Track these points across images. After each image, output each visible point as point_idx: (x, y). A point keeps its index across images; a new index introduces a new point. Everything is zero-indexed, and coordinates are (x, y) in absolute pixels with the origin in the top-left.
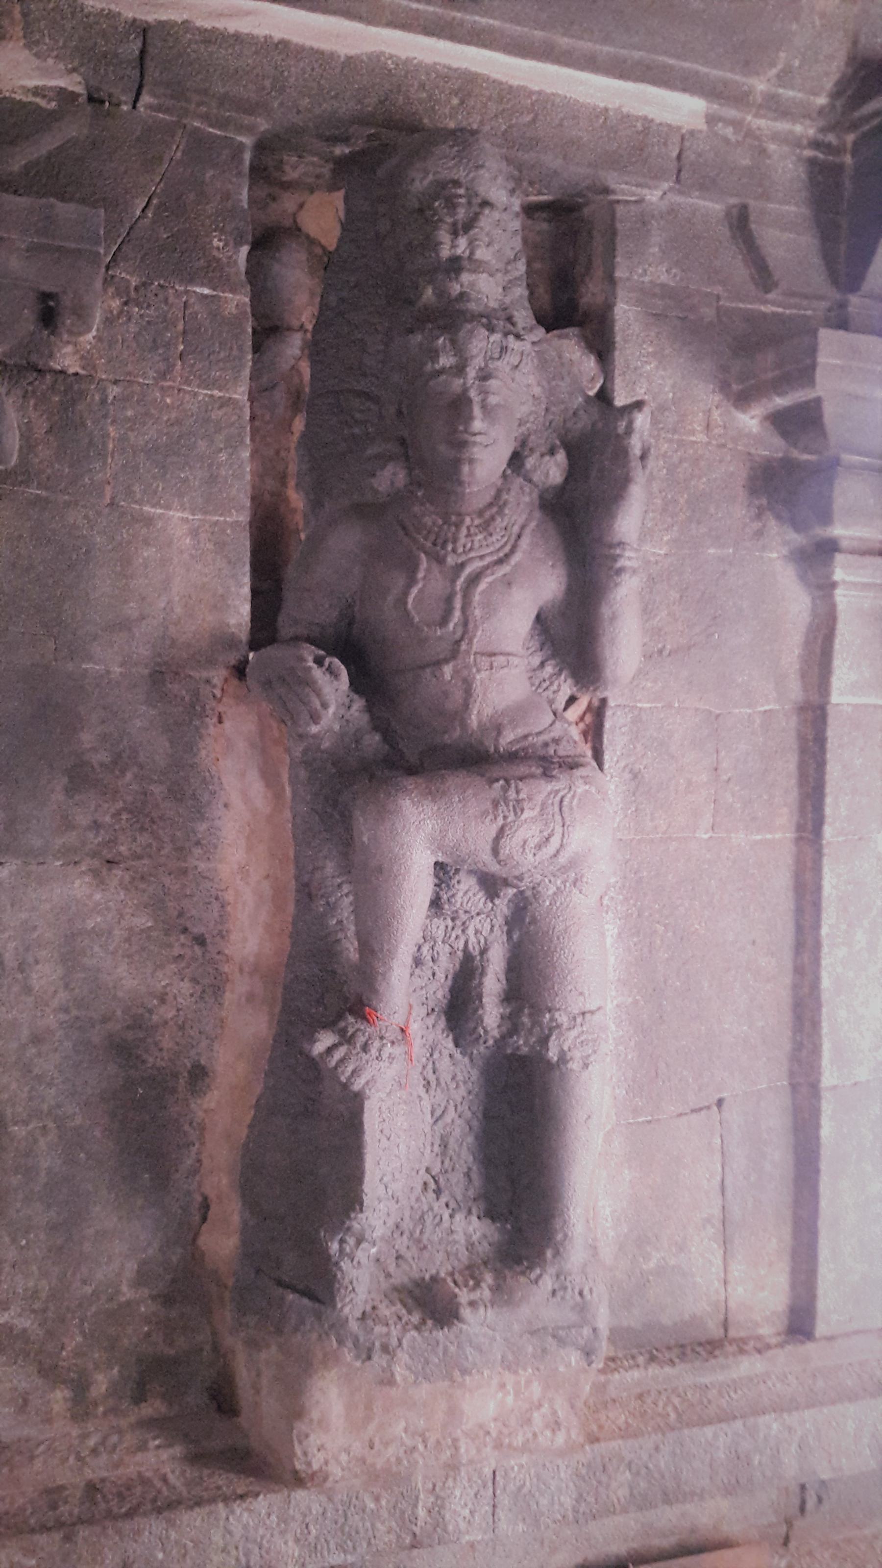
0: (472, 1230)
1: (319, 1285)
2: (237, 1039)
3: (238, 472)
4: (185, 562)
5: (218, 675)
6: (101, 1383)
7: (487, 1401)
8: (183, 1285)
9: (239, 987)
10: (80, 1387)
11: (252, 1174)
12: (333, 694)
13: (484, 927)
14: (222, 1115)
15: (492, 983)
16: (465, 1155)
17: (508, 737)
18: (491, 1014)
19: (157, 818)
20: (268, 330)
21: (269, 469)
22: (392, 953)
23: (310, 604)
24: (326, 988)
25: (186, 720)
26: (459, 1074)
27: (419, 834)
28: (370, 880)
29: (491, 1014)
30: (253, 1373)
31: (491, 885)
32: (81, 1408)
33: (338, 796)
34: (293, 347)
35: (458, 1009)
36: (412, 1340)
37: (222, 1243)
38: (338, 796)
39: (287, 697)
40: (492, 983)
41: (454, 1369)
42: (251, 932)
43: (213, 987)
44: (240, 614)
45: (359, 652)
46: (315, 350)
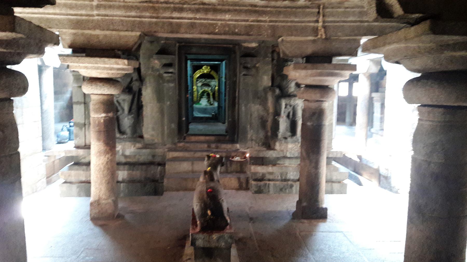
0: (289, 134)
1: (277, 136)
2: (270, 120)
3: (270, 73)
4: (266, 81)
5: (268, 89)
6: (260, 144)
7: (290, 146)
8: (266, 137)
9: (270, 114)
10: (259, 144)
11: (271, 129)
12: (277, 91)
13: (290, 109)
14: (269, 124)
15: (291, 114)
16: (289, 128)
17: (292, 94)
18: (291, 116)
19: (264, 102)
20: (273, 60)
21: (273, 71)
22: (233, 40)
23: (276, 83)
24: (277, 113)
25: (266, 93)
26: (289, 122)
27: (283, 103)
28: (280, 105)
29: (291, 116)
30: (272, 143)
31: (291, 106)
32: (259, 146)
33: (277, 99)
34: (275, 61)
35: (288, 116)
36: (283, 141)
37: (269, 134)
38: (277, 99)
39: (274, 91)
40: (291, 114)
41: (287, 143)
42: (271, 110)
43: (268, 114)
44: (270, 84)
45: (280, 87)
46: (277, 61)
